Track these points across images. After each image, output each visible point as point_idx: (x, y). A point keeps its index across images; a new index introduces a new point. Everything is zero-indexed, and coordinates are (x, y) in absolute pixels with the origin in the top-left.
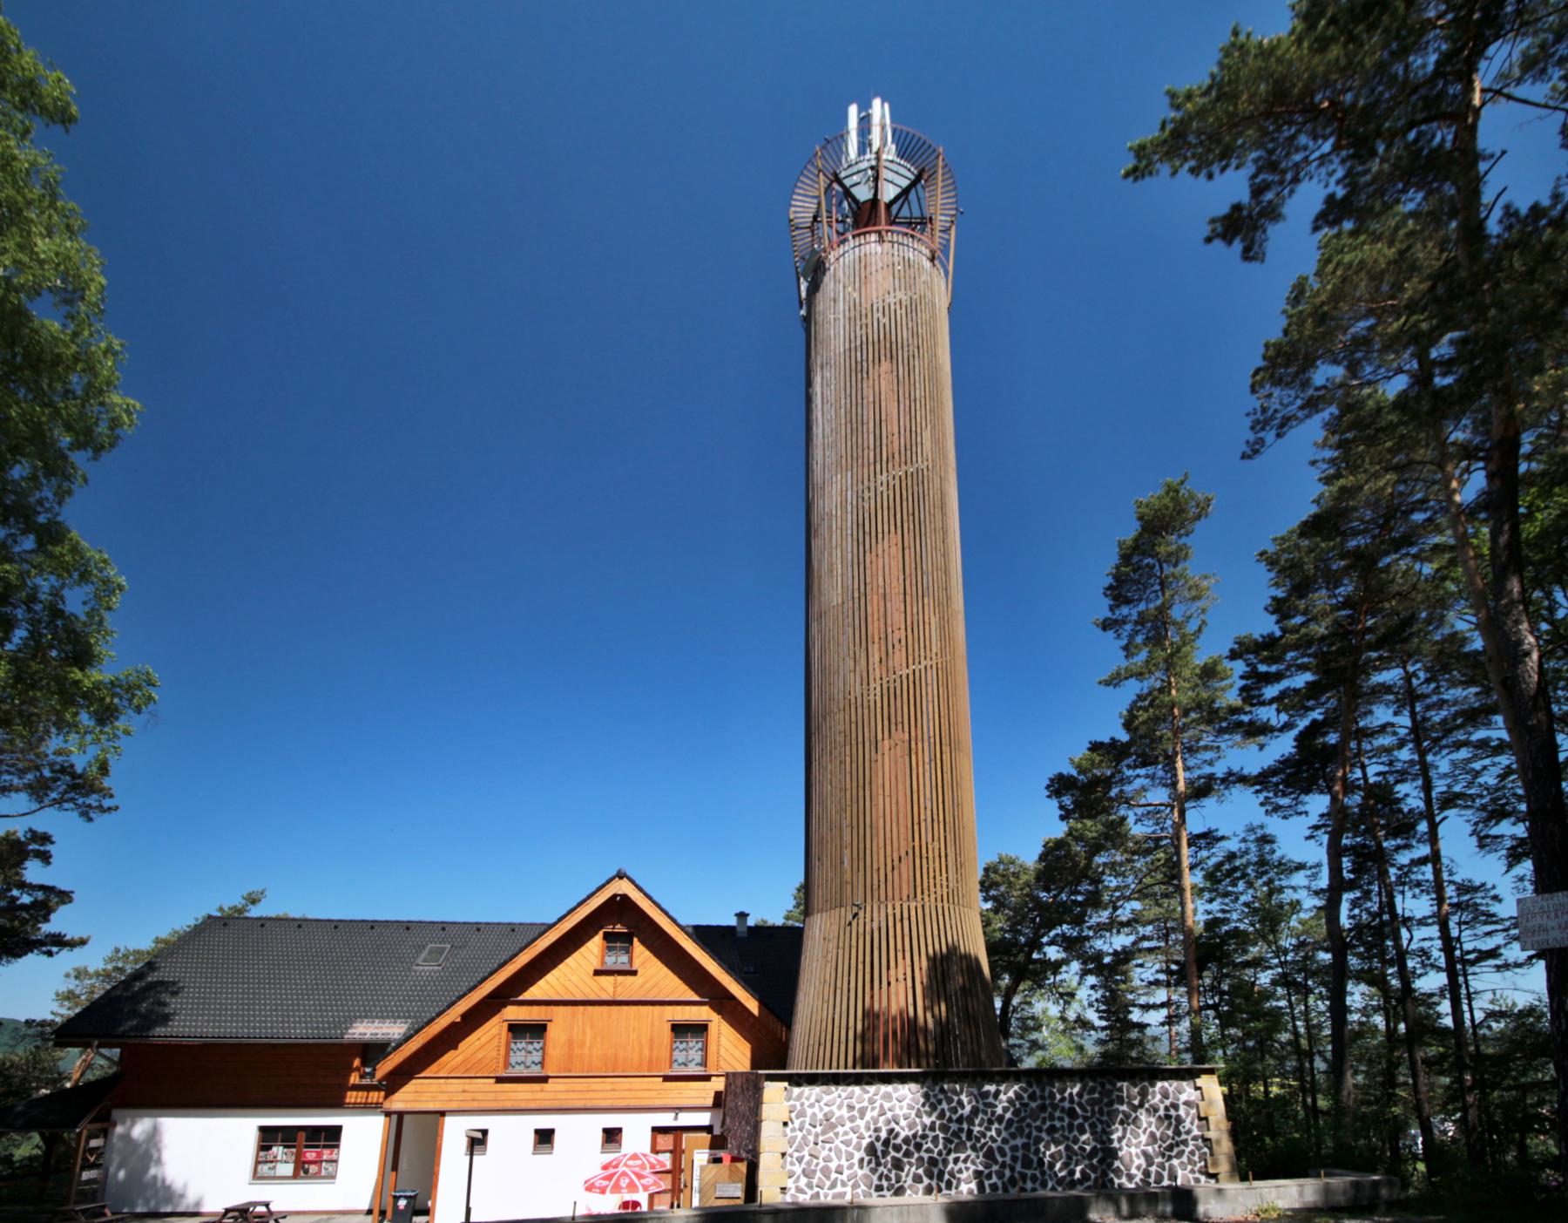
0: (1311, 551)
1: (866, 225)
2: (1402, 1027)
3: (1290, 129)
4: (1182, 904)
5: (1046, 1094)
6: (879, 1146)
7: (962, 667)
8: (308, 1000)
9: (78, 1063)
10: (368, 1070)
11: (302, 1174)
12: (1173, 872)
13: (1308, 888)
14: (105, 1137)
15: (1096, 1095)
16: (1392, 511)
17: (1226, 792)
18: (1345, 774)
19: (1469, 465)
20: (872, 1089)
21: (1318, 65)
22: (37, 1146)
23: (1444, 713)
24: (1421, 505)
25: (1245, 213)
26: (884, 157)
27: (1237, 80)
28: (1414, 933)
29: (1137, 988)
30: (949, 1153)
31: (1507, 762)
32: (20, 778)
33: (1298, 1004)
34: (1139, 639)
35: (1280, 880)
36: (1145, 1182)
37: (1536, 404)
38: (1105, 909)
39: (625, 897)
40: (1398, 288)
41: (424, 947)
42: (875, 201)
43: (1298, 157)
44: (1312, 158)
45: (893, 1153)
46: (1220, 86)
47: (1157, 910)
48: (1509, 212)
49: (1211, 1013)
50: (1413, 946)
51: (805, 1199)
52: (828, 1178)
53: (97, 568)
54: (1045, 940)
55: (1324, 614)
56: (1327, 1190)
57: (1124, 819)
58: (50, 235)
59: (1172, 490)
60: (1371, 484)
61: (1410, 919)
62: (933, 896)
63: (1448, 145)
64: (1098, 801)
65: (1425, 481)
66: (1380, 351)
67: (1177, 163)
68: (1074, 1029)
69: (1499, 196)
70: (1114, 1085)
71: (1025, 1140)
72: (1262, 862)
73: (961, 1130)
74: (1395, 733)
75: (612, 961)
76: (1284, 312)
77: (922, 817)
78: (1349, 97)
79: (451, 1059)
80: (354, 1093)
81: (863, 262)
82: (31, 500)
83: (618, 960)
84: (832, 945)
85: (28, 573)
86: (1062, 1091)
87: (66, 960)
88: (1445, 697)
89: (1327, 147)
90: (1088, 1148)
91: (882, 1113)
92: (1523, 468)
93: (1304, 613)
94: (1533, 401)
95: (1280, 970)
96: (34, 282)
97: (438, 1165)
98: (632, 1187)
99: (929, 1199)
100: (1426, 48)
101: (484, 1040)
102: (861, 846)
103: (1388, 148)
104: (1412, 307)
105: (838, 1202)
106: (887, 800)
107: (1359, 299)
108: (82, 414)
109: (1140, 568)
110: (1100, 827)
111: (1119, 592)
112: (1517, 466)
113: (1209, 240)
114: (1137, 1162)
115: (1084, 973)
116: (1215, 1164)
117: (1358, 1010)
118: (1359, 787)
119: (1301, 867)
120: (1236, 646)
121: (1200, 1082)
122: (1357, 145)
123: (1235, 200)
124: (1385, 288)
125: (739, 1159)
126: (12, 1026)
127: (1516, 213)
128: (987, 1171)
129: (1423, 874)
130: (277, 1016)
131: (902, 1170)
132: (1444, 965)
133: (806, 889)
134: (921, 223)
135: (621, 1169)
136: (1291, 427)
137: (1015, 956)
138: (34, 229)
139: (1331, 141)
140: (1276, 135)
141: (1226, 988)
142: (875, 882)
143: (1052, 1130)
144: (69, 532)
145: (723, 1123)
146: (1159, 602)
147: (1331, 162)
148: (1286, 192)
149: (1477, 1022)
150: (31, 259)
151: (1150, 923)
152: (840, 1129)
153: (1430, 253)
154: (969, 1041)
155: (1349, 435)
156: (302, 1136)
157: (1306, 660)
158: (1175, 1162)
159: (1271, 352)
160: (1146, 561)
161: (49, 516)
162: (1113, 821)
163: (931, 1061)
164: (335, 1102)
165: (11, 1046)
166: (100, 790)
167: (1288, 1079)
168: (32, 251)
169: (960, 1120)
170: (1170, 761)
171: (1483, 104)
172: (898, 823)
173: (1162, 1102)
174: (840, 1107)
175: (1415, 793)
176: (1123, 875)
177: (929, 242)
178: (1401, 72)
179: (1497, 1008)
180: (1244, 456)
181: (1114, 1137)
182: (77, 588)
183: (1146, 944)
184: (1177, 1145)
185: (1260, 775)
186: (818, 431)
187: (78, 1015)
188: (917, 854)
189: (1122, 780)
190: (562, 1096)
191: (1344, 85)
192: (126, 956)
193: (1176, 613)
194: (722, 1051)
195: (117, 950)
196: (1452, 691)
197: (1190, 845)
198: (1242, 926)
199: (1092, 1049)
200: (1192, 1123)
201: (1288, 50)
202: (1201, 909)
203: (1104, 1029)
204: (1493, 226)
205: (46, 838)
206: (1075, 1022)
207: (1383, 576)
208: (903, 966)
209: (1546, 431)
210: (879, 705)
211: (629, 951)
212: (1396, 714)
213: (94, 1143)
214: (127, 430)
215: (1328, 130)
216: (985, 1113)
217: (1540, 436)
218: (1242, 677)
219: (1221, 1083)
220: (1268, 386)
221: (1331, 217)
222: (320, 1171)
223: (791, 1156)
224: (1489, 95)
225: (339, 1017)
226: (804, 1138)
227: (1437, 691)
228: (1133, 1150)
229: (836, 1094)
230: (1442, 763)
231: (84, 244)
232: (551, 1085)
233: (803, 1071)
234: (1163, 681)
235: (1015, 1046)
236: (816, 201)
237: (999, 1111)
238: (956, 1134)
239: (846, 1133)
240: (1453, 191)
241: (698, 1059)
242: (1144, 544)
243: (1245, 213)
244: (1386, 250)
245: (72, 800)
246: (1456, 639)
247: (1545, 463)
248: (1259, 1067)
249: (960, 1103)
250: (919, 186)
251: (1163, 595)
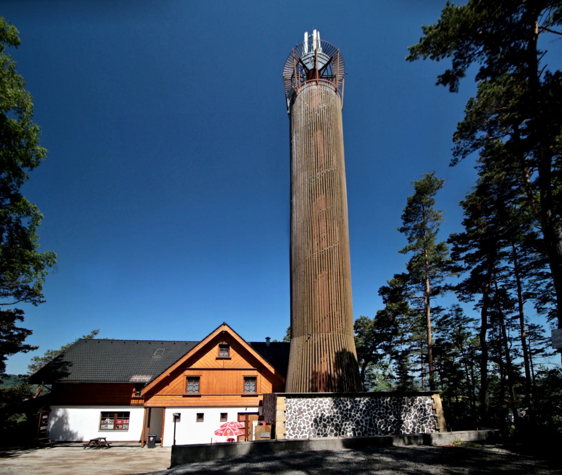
0: (480, 201)
1: (311, 79)
2: (507, 377)
3: (467, 42)
4: (428, 334)
5: (378, 401)
6: (318, 419)
7: (347, 246)
8: (116, 368)
9: (37, 390)
10: (138, 392)
11: (116, 428)
12: (424, 322)
13: (474, 328)
14: (48, 415)
15: (396, 402)
16: (504, 185)
17: (445, 293)
18: (489, 286)
19: (533, 169)
20: (315, 399)
21: (478, 17)
22: (25, 418)
23: (527, 263)
24: (514, 184)
25: (451, 74)
26: (318, 52)
27: (448, 23)
28: (512, 343)
29: (411, 364)
30: (343, 422)
31: (550, 281)
32: (11, 291)
33: (469, 369)
34: (414, 235)
35: (464, 324)
36: (413, 432)
37: (557, 146)
38: (399, 335)
39: (226, 332)
40: (507, 103)
41: (156, 350)
42: (314, 69)
43: (470, 53)
44: (476, 53)
45: (323, 422)
46: (442, 25)
47: (418, 336)
48: (548, 74)
49: (437, 372)
50: (512, 348)
51: (292, 438)
52: (300, 430)
53: (32, 210)
54: (377, 347)
55: (484, 226)
56: (479, 435)
57: (407, 303)
58: (12, 87)
59: (429, 178)
60: (497, 175)
61: (511, 338)
62: (337, 331)
63: (526, 48)
64: (398, 296)
65: (516, 174)
66: (500, 126)
67: (426, 55)
68: (388, 378)
69: (544, 68)
70: (402, 398)
71: (370, 417)
72: (457, 318)
73: (347, 414)
74: (508, 270)
75: (222, 355)
76: (465, 111)
77: (333, 303)
78: (489, 30)
79: (167, 389)
80: (134, 401)
81: (310, 93)
82: (8, 185)
83: (224, 354)
85: (8, 212)
86: (383, 400)
87: (31, 354)
88: (528, 256)
89: (481, 49)
90: (393, 420)
91: (319, 408)
92: (552, 169)
93: (477, 225)
94: (556, 145)
95: (463, 357)
96: (7, 105)
97: (164, 425)
98: (231, 434)
99: (336, 438)
100: (518, 11)
101: (178, 382)
102: (311, 313)
103: (503, 50)
104: (512, 109)
105: (303, 439)
106: (320, 296)
107: (493, 107)
108: (26, 154)
109: (415, 208)
110: (398, 306)
111: (407, 217)
112: (550, 169)
113: (437, 84)
114: (410, 425)
115: (392, 358)
116: (438, 426)
117: (491, 371)
118: (494, 291)
119: (471, 320)
120: (450, 238)
121: (433, 397)
122: (491, 48)
123: (447, 69)
124: (502, 102)
125: (269, 424)
126: (14, 377)
127: (551, 74)
128: (356, 428)
129: (516, 322)
130: (105, 374)
131: (326, 428)
132: (523, 355)
133: (291, 329)
134: (332, 78)
135: (227, 427)
136: (468, 154)
137: (367, 352)
138: (6, 85)
139: (483, 46)
140: (462, 44)
141: (443, 364)
142: (316, 326)
144: (22, 197)
145: (263, 412)
146: (422, 221)
147: (483, 54)
148: (466, 66)
149: (535, 375)
150: (6, 97)
151: (416, 340)
152: (304, 414)
153: (519, 89)
154: (350, 383)
155: (489, 157)
156: (116, 415)
157: (476, 243)
158: (424, 425)
159: (460, 126)
160: (418, 205)
161: (15, 191)
162: (403, 304)
163: (337, 390)
164: (127, 404)
165: (14, 384)
166: (39, 295)
167: (465, 396)
168: (6, 94)
169: (347, 410)
170: (424, 282)
171: (539, 33)
172: (324, 305)
173: (419, 404)
174: (304, 406)
175: (515, 293)
176: (406, 323)
177: (335, 85)
178: (509, 20)
179: (541, 370)
180: (450, 165)
181: (402, 416)
182: (25, 218)
183: (414, 348)
184: (425, 419)
185: (457, 286)
186: (294, 156)
187: (36, 373)
188: (331, 316)
189: (406, 289)
190: (206, 402)
191: (488, 25)
192: (52, 353)
193: (428, 225)
194: (262, 386)
195: (49, 351)
196: (530, 255)
197: (431, 312)
198: (449, 341)
199: (394, 386)
200: (430, 411)
201: (467, 11)
202: (434, 336)
203: (398, 378)
204: (542, 79)
205: (21, 312)
206: (388, 376)
207: (507, 210)
208: (326, 356)
209: (561, 156)
210: (317, 261)
211: (228, 351)
212: (509, 263)
213: (44, 417)
214: (42, 159)
215: (482, 42)
217: (559, 158)
218: (452, 250)
219: (441, 397)
220: (459, 139)
221: (482, 76)
222: (123, 427)
223: (287, 423)
224: (541, 30)
225: (127, 374)
226: (292, 416)
227: (525, 254)
228: (409, 421)
229: (303, 401)
230: (526, 281)
231: (25, 90)
232: (202, 398)
233: (291, 393)
234: (422, 251)
235: (366, 384)
236: (293, 69)
237: (361, 407)
238: (345, 415)
239: (306, 415)
240: (527, 66)
241: (254, 389)
242: (417, 199)
243: (451, 74)
244: (502, 88)
245: (29, 298)
246: (533, 235)
247: (560, 168)
248: (454, 391)
250: (331, 64)
251: (424, 218)
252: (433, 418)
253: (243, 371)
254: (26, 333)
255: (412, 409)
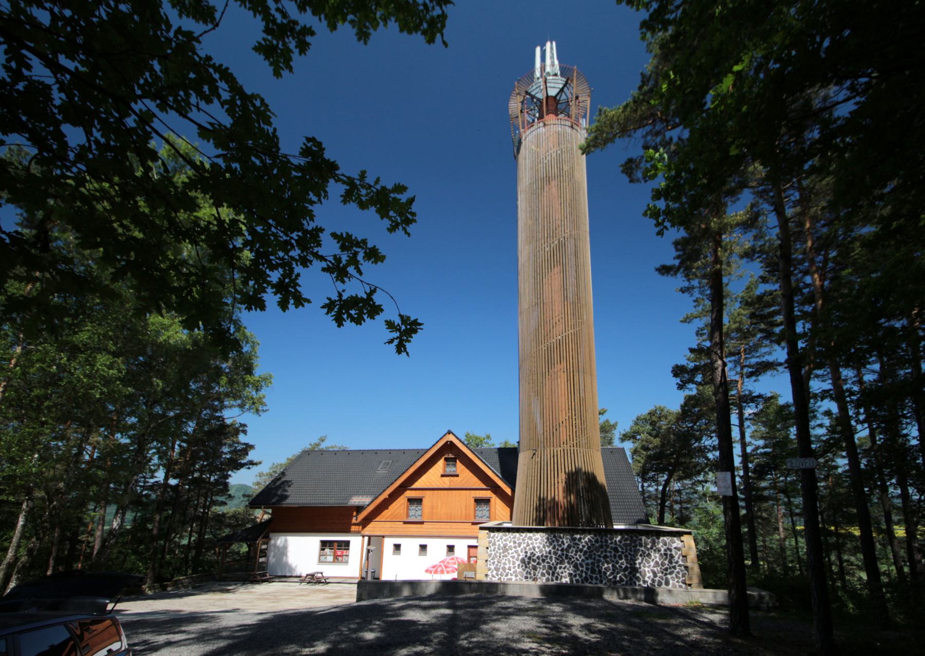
6: (526, 560)
20: (524, 535)
30: (557, 564)
39: (451, 442)
45: (532, 563)
71: (592, 561)
79: (386, 514)
83: (450, 470)
84: (526, 468)
86: (611, 539)
87: (255, 469)
90: (623, 566)
91: (528, 545)
105: (499, 581)
114: (648, 575)
116: (690, 579)
121: (682, 538)
128: (574, 573)
143: (605, 557)
152: (510, 551)
156: (336, 544)
158: (669, 576)
164: (346, 530)
174: (510, 542)
181: (637, 562)
192: (277, 467)
200: (679, 558)
205: (245, 425)
211: (455, 465)
216: (574, 547)
226: (495, 554)
237: (581, 547)
239: (512, 553)
241: (488, 515)
249: (563, 542)
252: (683, 568)
253: (473, 492)
254: (248, 447)
255: (652, 554)
